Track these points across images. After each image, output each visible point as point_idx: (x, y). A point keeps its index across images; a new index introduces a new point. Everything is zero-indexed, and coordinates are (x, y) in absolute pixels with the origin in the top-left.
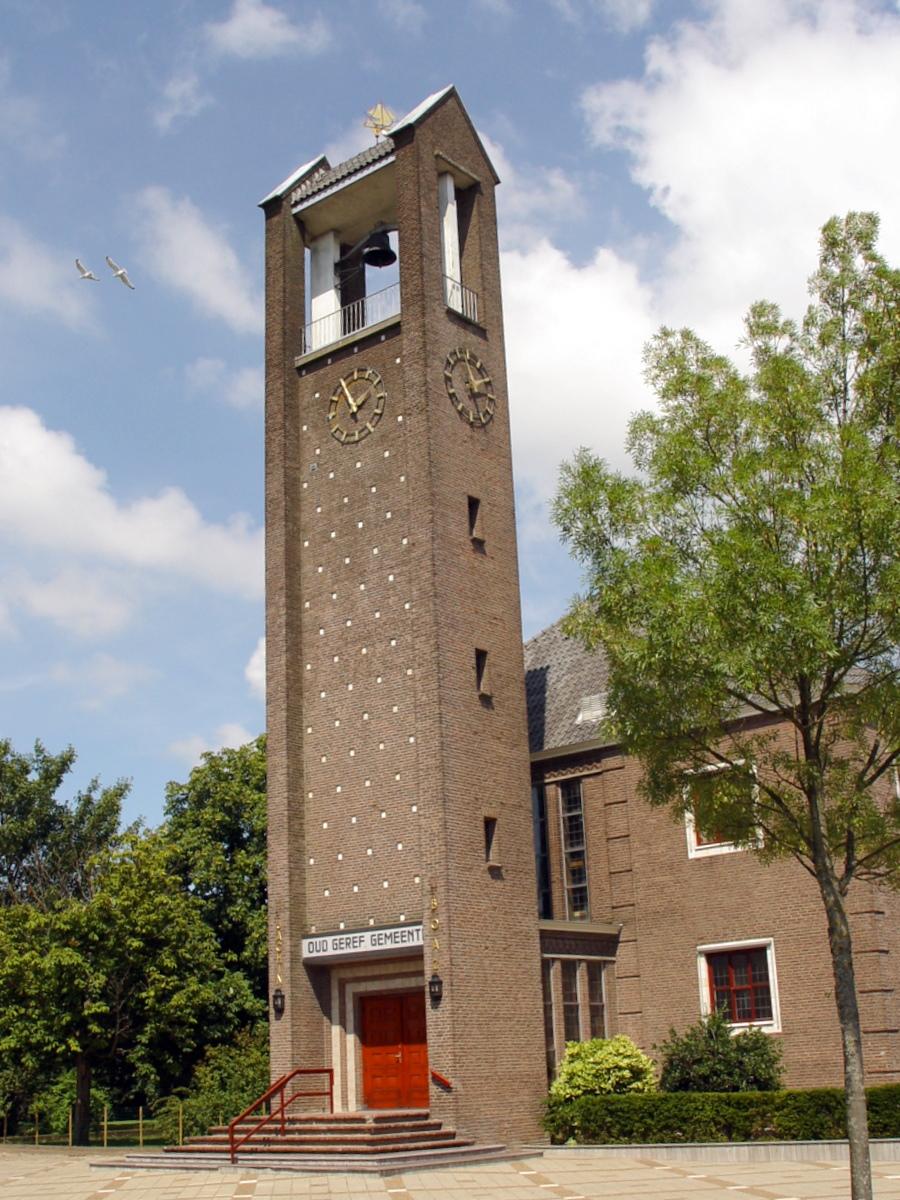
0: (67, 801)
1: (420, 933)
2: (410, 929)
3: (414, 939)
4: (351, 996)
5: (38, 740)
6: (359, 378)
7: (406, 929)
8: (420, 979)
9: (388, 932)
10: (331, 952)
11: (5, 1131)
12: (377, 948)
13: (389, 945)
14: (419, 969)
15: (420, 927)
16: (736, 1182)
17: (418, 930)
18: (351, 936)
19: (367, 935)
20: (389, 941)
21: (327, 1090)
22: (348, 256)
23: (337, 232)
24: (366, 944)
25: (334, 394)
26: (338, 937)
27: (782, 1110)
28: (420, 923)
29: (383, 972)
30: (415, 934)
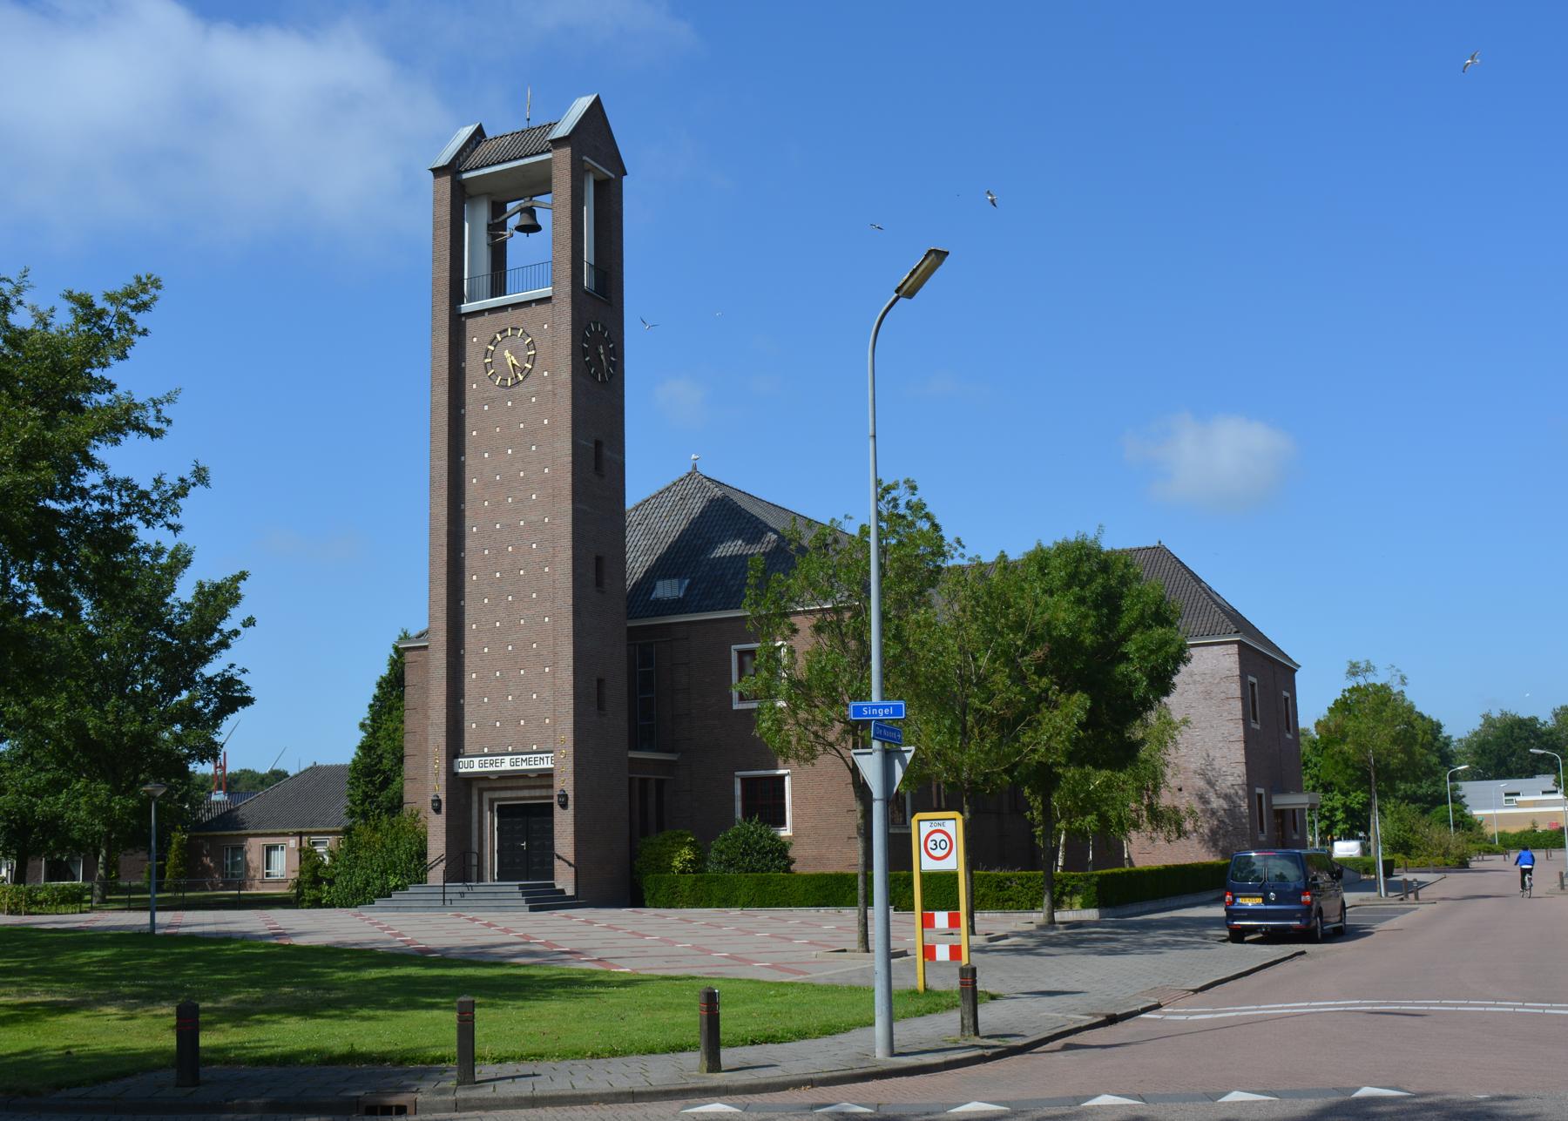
0: (161, 526)
1: (549, 759)
2: (542, 756)
3: (546, 763)
4: (487, 801)
5: (243, 576)
6: (502, 339)
7: (539, 756)
8: (550, 790)
9: (524, 757)
10: (476, 769)
11: (904, 831)
12: (515, 768)
13: (524, 766)
14: (550, 794)
15: (550, 755)
16: (560, 945)
17: (547, 757)
18: (494, 758)
19: (507, 759)
20: (524, 764)
21: (971, 953)
22: (496, 221)
23: (489, 194)
24: (506, 764)
25: (491, 344)
26: (484, 759)
27: (1418, 779)
28: (551, 752)
29: (514, 785)
30: (545, 759)
